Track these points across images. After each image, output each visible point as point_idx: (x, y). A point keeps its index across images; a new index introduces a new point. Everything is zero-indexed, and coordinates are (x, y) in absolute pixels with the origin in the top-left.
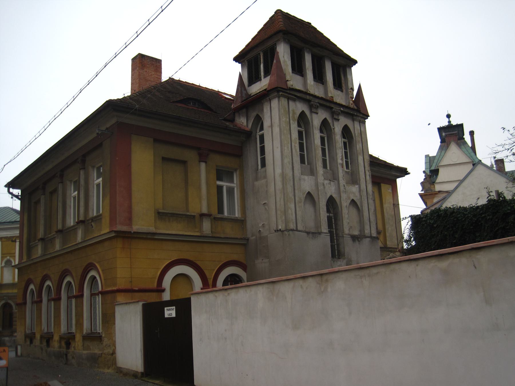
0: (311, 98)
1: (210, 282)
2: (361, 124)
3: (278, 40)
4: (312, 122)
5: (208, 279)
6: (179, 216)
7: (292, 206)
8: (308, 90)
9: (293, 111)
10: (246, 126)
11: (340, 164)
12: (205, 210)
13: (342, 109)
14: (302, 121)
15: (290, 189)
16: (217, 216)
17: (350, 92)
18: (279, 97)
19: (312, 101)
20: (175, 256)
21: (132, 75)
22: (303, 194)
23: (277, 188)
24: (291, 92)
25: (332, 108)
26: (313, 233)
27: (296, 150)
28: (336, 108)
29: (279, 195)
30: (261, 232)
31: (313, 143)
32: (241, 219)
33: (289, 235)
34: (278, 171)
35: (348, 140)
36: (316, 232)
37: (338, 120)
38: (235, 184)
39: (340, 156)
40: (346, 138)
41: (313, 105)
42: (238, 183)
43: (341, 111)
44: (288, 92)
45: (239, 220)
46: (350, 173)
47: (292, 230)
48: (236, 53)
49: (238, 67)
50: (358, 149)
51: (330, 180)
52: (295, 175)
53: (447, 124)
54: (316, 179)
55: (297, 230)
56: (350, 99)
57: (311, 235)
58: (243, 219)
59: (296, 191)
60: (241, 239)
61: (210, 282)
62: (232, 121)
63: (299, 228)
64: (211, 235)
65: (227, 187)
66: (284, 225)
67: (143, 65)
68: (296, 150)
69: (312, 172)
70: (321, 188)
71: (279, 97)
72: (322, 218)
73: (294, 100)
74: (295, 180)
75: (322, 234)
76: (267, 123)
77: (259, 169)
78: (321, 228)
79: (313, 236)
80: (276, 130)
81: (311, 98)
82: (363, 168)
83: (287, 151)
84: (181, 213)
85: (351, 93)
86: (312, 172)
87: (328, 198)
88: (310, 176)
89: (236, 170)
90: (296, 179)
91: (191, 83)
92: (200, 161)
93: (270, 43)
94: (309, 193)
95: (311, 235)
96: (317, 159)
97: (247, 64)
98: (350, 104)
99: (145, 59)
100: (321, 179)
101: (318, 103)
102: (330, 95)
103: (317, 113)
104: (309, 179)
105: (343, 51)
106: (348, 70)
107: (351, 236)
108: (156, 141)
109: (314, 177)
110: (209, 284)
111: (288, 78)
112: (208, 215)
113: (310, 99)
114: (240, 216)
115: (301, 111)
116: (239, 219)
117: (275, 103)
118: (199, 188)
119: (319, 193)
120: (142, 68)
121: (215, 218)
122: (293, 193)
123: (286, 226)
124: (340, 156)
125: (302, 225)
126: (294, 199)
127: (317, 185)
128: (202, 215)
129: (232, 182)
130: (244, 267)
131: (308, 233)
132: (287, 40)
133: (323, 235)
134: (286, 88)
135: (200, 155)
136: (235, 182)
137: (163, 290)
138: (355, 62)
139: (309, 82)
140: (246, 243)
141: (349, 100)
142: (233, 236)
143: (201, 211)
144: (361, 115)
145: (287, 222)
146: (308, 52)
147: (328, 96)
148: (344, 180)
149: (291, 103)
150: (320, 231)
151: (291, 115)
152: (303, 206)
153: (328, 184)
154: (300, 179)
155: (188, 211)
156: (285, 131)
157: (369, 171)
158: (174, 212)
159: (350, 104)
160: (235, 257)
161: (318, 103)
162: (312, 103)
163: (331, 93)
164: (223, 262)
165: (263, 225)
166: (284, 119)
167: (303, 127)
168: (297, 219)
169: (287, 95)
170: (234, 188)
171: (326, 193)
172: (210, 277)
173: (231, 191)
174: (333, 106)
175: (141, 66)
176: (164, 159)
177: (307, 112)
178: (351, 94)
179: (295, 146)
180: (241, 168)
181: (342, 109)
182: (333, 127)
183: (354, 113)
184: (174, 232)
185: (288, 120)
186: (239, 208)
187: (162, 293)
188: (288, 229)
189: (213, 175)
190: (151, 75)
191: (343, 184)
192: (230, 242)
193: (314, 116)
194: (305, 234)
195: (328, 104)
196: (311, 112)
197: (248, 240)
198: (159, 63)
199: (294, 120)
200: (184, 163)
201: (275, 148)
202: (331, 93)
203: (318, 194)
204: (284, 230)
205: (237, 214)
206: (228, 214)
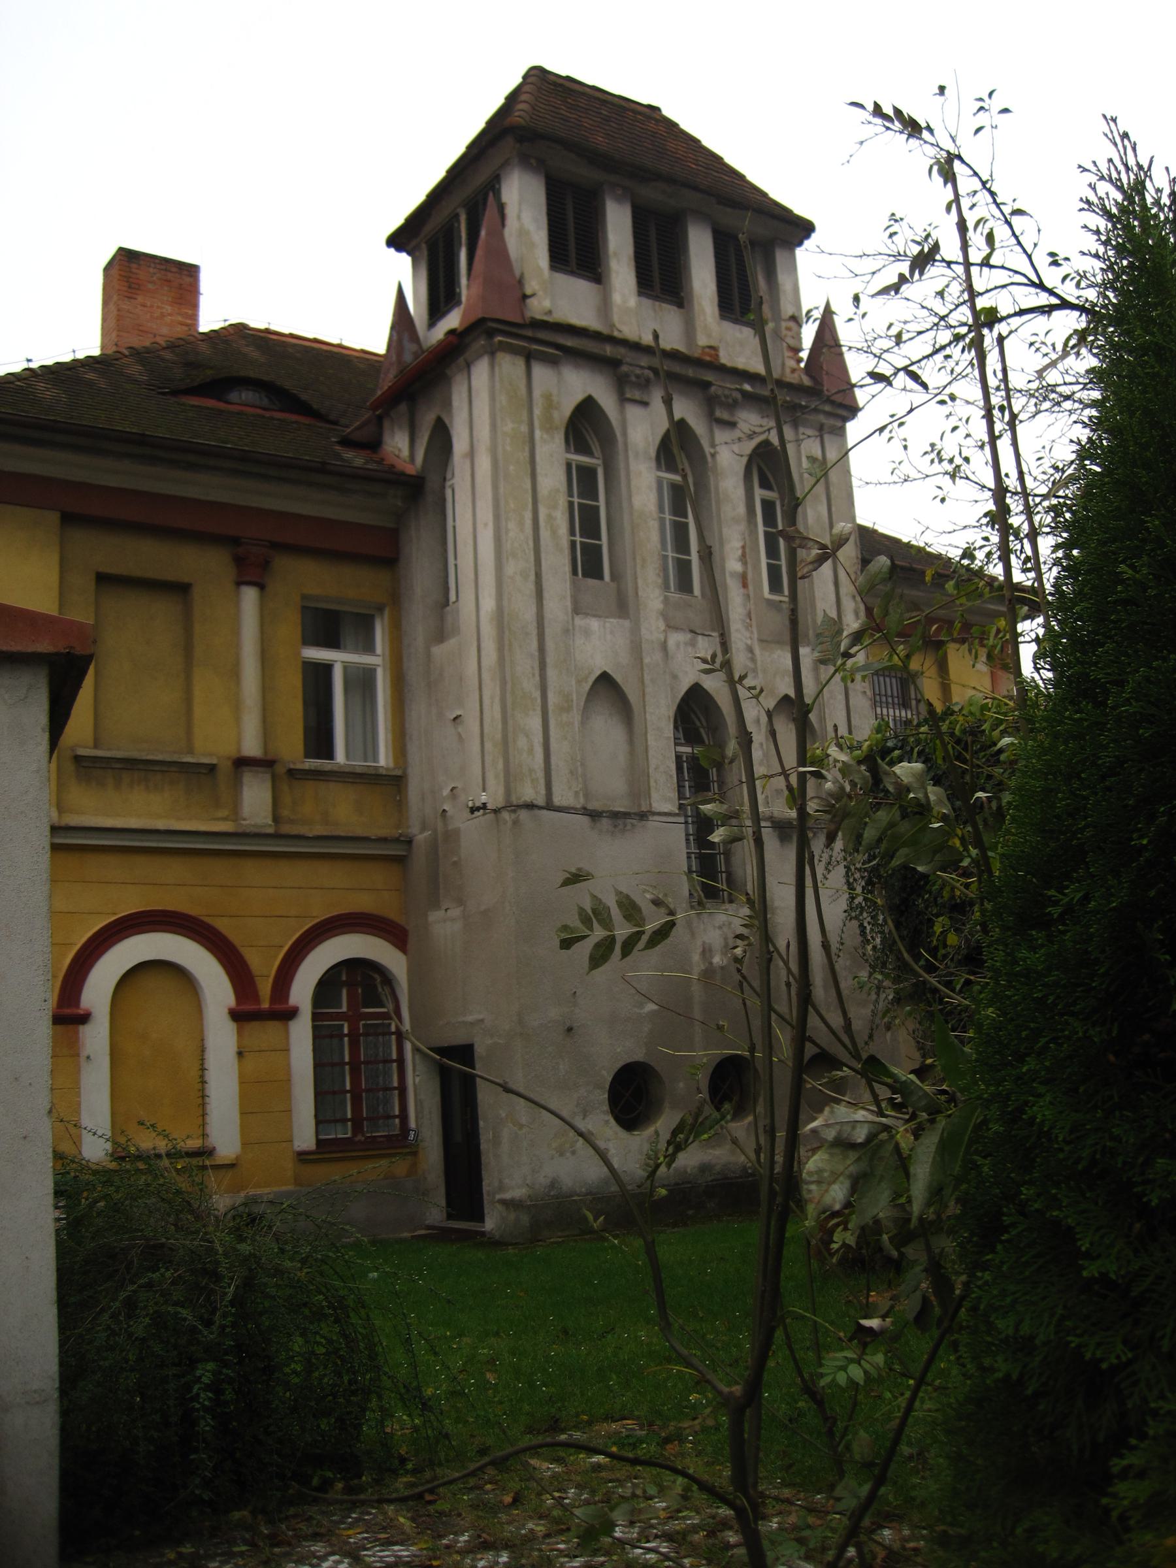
0: (620, 352)
1: (265, 988)
2: (826, 437)
3: (506, 164)
4: (625, 434)
5: (256, 978)
6: (347, 780)
7: (535, 723)
8: (613, 326)
9: (548, 398)
10: (407, 459)
11: (733, 574)
12: (251, 747)
13: (747, 387)
14: (589, 429)
15: (524, 664)
16: (299, 766)
17: (789, 329)
18: (492, 354)
19: (627, 364)
20: (131, 903)
21: (104, 320)
22: (579, 682)
23: (485, 662)
24: (542, 335)
25: (707, 385)
26: (615, 815)
27: (554, 532)
28: (721, 386)
29: (491, 689)
30: (449, 814)
31: (625, 504)
32: (394, 773)
33: (516, 822)
34: (488, 604)
35: (779, 493)
36: (635, 810)
37: (732, 425)
38: (377, 660)
39: (737, 549)
40: (775, 488)
41: (627, 375)
42: (387, 653)
43: (745, 394)
44: (529, 333)
45: (382, 775)
46: (785, 606)
47: (530, 806)
48: (397, 220)
49: (402, 264)
50: (810, 521)
51: (692, 631)
52: (548, 615)
53: (854, 381)
54: (635, 630)
55: (550, 806)
56: (788, 354)
57: (605, 823)
58: (398, 773)
59: (551, 673)
60: (383, 840)
61: (265, 988)
62: (374, 445)
63: (557, 800)
64: (271, 831)
65: (346, 668)
66: (501, 791)
67: (133, 286)
68: (554, 532)
69: (623, 606)
70: (652, 658)
71: (492, 354)
72: (653, 763)
73: (553, 362)
74: (548, 631)
75: (651, 818)
76: (460, 445)
77: (450, 603)
78: (650, 797)
79: (615, 826)
80: (484, 464)
81: (620, 352)
82: (832, 588)
83: (518, 535)
84: (160, 757)
85: (789, 333)
86: (623, 606)
87: (682, 693)
88: (607, 617)
89: (380, 609)
90: (552, 631)
91: (311, 336)
92: (239, 584)
93: (479, 179)
94: (605, 679)
95: (605, 823)
96: (639, 561)
97: (425, 253)
98: (788, 371)
99: (139, 265)
100: (652, 627)
101: (650, 368)
102: (702, 341)
103: (645, 404)
104: (604, 627)
105: (765, 195)
106: (780, 256)
107: (773, 822)
108: (69, 519)
109: (627, 623)
110: (261, 993)
111: (531, 286)
112: (265, 763)
113: (619, 357)
114: (391, 765)
115: (579, 397)
116: (384, 773)
117: (481, 372)
118: (235, 673)
119: (645, 676)
120: (130, 295)
121: (292, 773)
122: (537, 678)
123: (508, 792)
124: (737, 549)
125: (570, 788)
126: (539, 700)
127: (636, 648)
128: (242, 763)
129: (369, 648)
130: (397, 935)
131: (594, 815)
132: (533, 161)
133: (653, 823)
134: (519, 320)
135: (240, 562)
136: (379, 649)
137: (291, 1014)
138: (805, 229)
139: (617, 298)
140: (404, 853)
141: (783, 357)
142: (359, 832)
143: (239, 750)
144: (827, 408)
145: (510, 778)
146: (619, 200)
147: (697, 345)
148: (752, 632)
149: (540, 372)
150: (644, 809)
151: (537, 412)
152: (577, 724)
153: (686, 644)
154: (566, 631)
155: (191, 751)
156: (511, 468)
157: (854, 597)
158: (135, 754)
159: (788, 371)
160: (363, 903)
161: (650, 368)
162: (625, 368)
163: (709, 336)
164: (318, 920)
165: (452, 790)
166: (509, 427)
167: (596, 449)
168: (553, 767)
169: (526, 345)
170: (375, 670)
171: (675, 677)
172: (264, 967)
173: (362, 682)
174: (709, 377)
175: (125, 289)
176: (104, 580)
177: (607, 401)
178: (793, 337)
179: (550, 518)
180: (395, 600)
181: (747, 387)
182: (712, 451)
183: (797, 401)
184: (134, 823)
185: (524, 428)
186: (390, 736)
187: (81, 1028)
188: (515, 803)
189: (290, 627)
190: (163, 315)
191: (747, 645)
192: (322, 850)
193: (633, 411)
194: (585, 820)
195: (690, 372)
196: (623, 400)
197: (409, 842)
198: (191, 276)
199: (549, 427)
200: (181, 590)
201: (480, 526)
202: (709, 336)
203: (643, 682)
204: (500, 806)
205: (384, 759)
206: (348, 757)
